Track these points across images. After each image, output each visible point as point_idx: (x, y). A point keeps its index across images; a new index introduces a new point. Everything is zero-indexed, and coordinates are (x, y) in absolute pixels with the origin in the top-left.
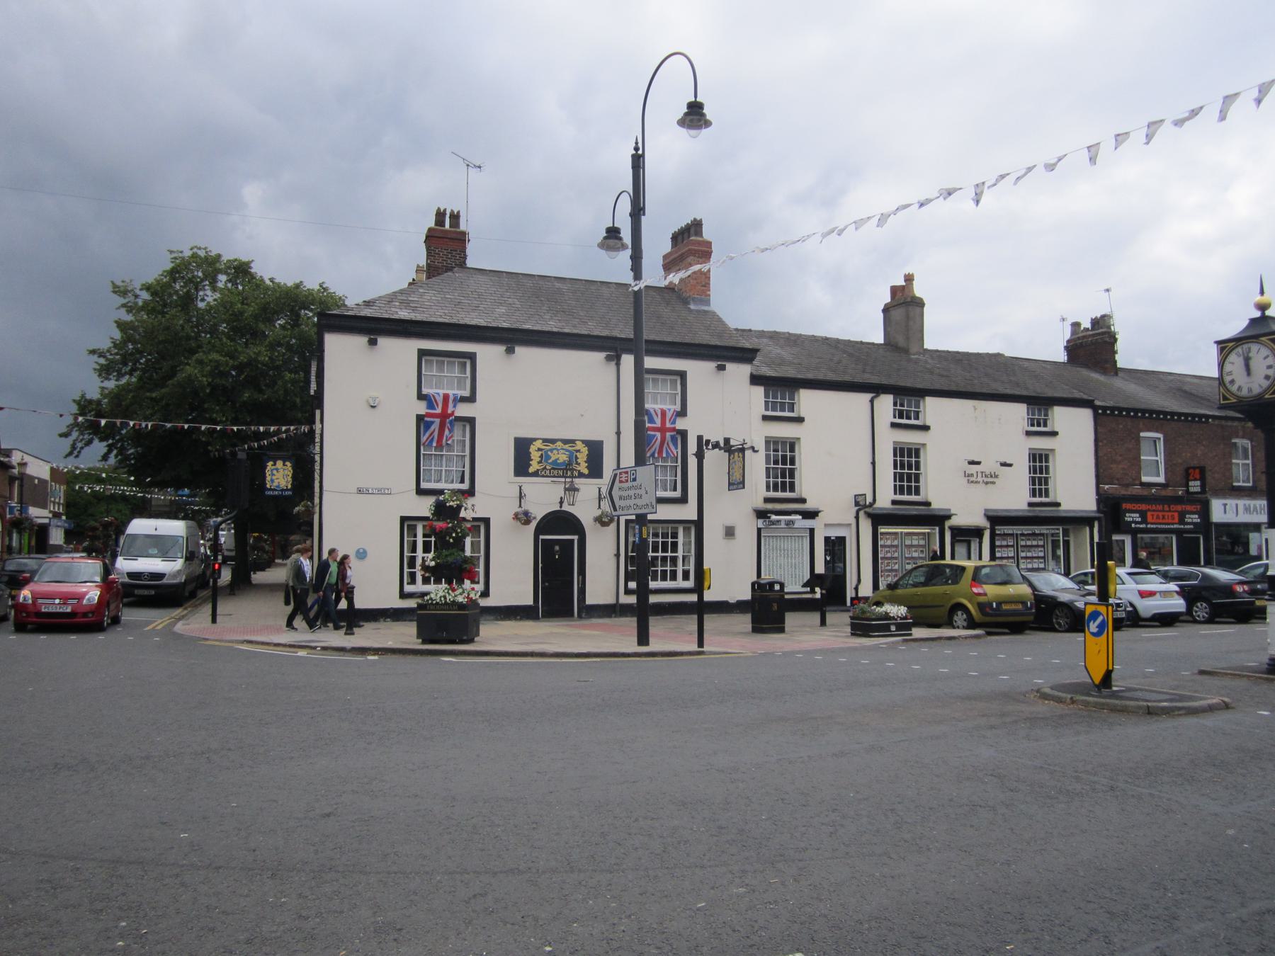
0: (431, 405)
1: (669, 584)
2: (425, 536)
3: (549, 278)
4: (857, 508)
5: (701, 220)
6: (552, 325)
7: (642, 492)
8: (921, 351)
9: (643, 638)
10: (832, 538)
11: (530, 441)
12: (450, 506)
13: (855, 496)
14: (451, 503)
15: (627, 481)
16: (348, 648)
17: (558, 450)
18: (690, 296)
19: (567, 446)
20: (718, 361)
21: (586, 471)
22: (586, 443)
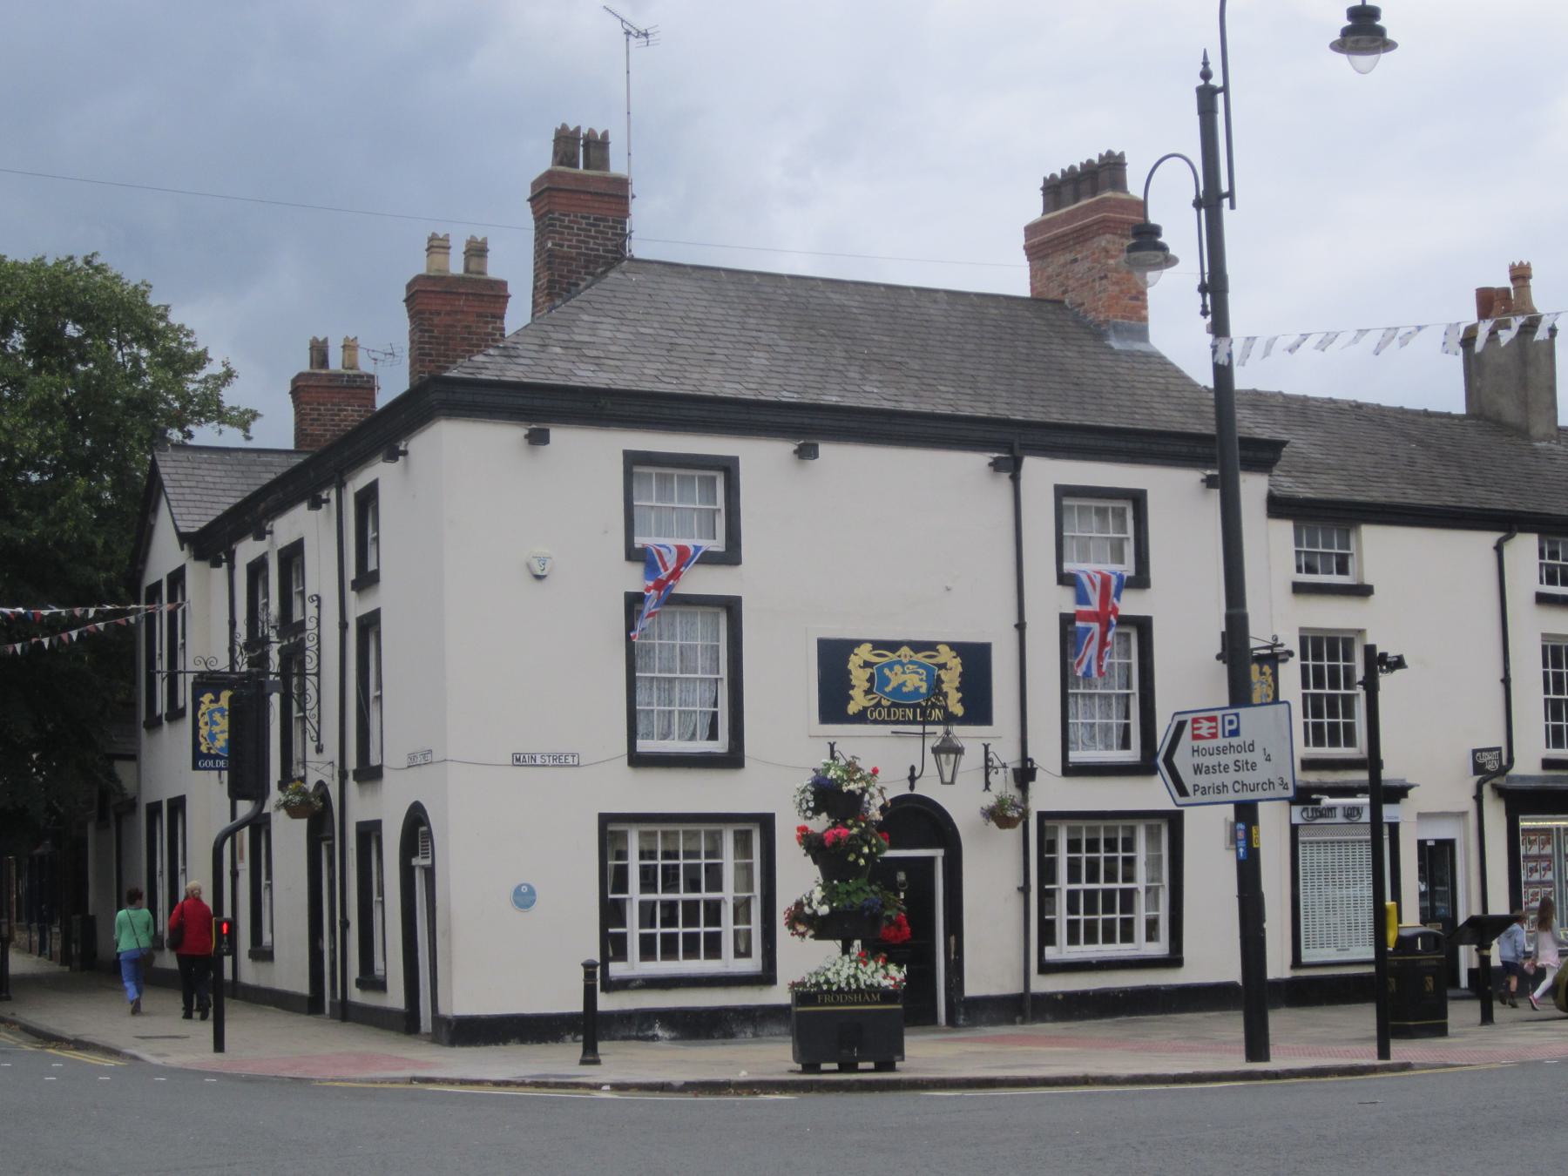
0: (1082, 598)
1: (701, 966)
2: (642, 855)
3: (813, 283)
4: (1478, 777)
5: (1122, 156)
6: (873, 395)
7: (1256, 757)
8: (1554, 432)
9: (1257, 1046)
10: (1429, 843)
11: (850, 645)
12: (849, 791)
13: (1475, 752)
14: (852, 786)
15: (1214, 736)
16: (676, 1084)
17: (903, 665)
18: (1107, 321)
19: (920, 655)
20: (1207, 467)
21: (958, 710)
22: (958, 648)
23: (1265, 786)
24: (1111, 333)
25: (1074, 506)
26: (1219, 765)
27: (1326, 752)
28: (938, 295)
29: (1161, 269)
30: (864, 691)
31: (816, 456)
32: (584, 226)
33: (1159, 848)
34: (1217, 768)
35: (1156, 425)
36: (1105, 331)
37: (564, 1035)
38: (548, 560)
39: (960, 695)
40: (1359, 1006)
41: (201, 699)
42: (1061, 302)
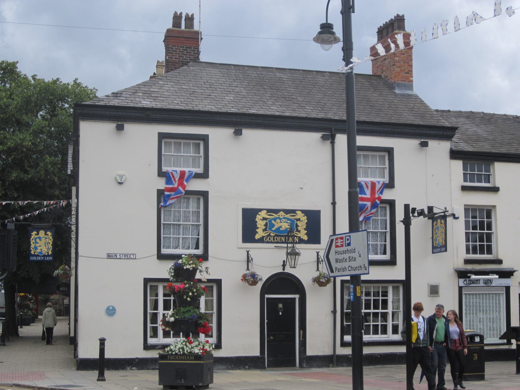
5: (403, 16)
6: (275, 110)
7: (355, 255)
11: (256, 212)
12: (187, 269)
14: (188, 267)
15: (342, 246)
17: (280, 219)
19: (288, 215)
21: (305, 238)
23: (359, 268)
24: (396, 87)
25: (361, 155)
26: (344, 259)
27: (478, 256)
28: (325, 74)
29: (332, 44)
30: (263, 230)
31: (241, 134)
32: (181, 50)
33: (399, 296)
34: (343, 260)
35: (399, 121)
36: (394, 86)
37: (126, 367)
38: (124, 176)
39: (306, 232)
40: (501, 362)
41: (32, 234)
42: (380, 76)
